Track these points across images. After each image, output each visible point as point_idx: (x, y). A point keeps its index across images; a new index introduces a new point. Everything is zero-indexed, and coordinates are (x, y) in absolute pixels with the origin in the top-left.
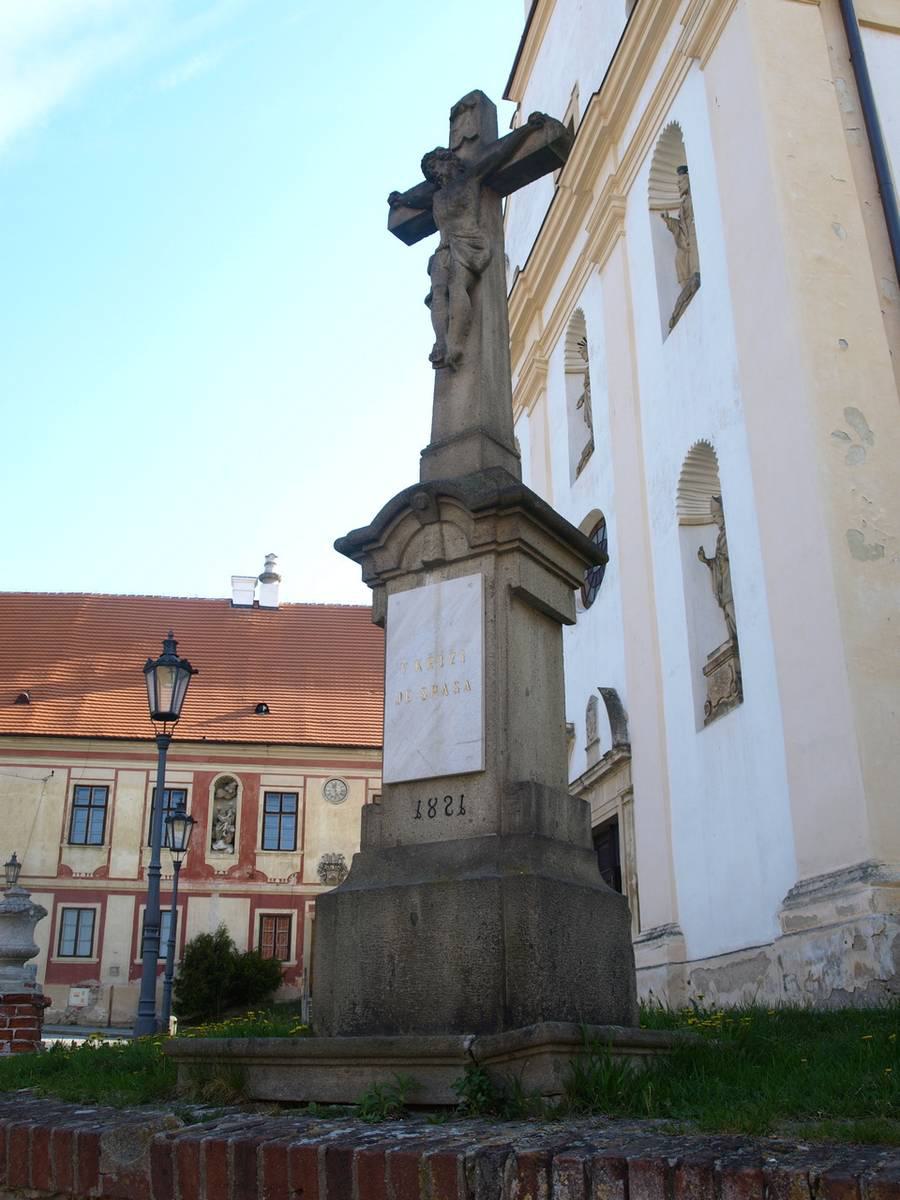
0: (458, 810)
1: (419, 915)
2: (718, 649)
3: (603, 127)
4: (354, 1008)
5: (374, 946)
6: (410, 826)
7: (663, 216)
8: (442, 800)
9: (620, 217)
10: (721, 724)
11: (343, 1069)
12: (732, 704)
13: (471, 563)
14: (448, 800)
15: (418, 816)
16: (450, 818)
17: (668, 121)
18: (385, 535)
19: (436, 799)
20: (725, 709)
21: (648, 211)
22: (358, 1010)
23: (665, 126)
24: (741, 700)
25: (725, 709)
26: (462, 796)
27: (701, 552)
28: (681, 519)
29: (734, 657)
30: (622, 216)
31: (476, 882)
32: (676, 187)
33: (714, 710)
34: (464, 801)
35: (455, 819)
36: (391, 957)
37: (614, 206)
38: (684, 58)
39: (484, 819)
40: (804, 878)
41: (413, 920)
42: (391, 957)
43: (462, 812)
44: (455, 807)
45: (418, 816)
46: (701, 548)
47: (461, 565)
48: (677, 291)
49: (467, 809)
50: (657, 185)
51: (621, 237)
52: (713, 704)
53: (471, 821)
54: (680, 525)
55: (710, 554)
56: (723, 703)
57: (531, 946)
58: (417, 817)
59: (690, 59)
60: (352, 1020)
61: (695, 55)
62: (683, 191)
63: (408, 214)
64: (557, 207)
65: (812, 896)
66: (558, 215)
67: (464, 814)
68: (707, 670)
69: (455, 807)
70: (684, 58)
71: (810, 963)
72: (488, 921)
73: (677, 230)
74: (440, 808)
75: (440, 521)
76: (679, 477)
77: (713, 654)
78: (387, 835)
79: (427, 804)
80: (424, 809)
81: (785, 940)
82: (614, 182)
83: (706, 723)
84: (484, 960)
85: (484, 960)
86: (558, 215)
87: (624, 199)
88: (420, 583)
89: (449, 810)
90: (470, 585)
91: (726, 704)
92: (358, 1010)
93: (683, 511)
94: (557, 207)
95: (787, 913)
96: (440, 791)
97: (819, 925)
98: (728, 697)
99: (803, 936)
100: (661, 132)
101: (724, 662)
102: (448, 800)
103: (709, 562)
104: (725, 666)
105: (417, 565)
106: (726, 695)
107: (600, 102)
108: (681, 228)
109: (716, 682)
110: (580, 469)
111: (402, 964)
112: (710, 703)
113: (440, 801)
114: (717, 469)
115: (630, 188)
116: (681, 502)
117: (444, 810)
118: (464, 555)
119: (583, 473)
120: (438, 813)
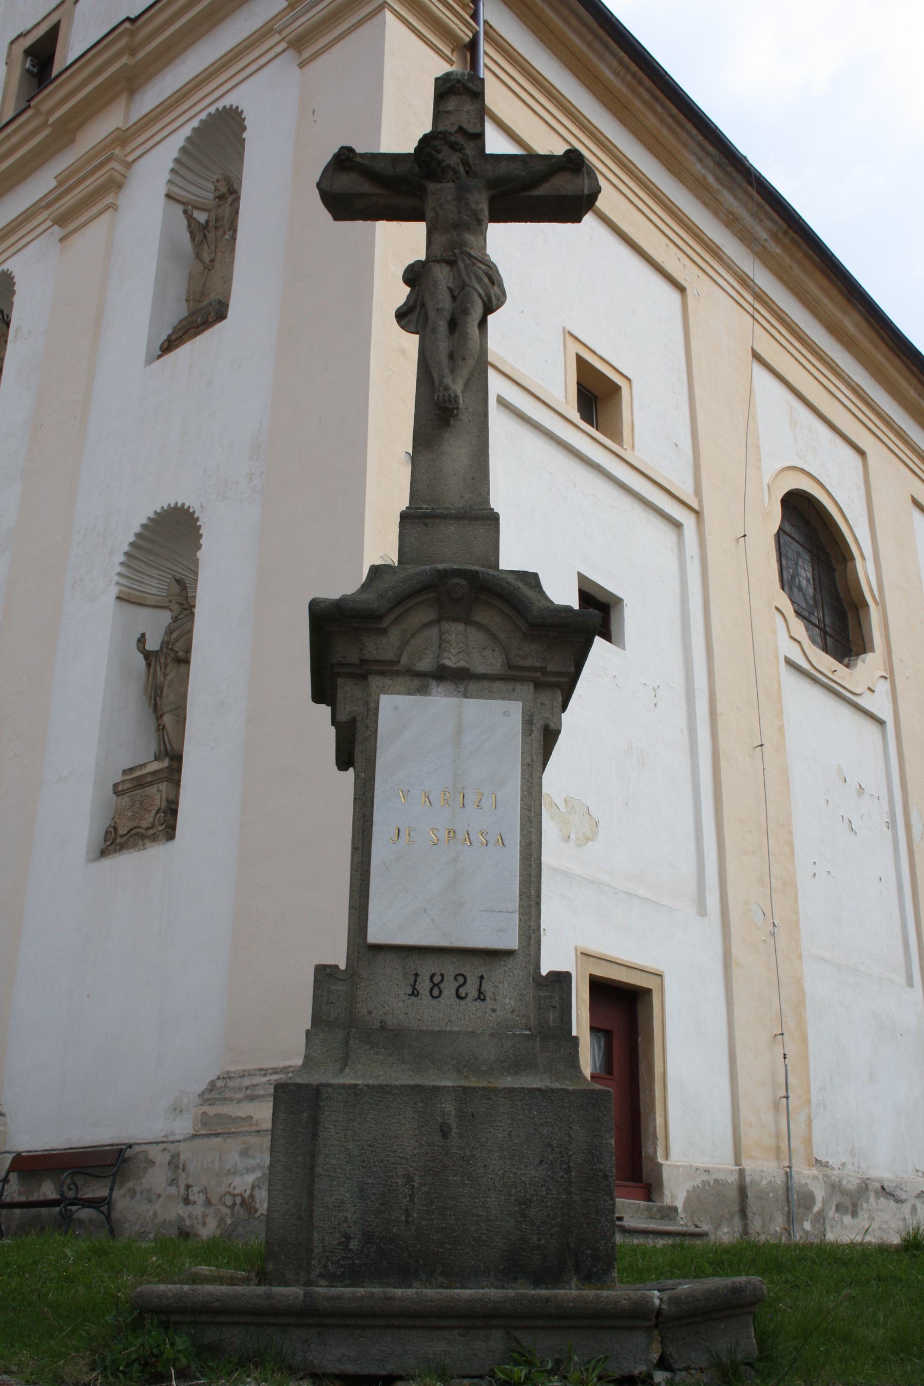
0: (474, 993)
1: (454, 1126)
2: (144, 765)
3: (126, 65)
4: (349, 1243)
5: (382, 1161)
6: (401, 1004)
7: (185, 212)
8: (451, 979)
9: (115, 185)
10: (127, 862)
11: (456, 1332)
12: (154, 838)
13: (498, 685)
14: (461, 980)
15: (415, 993)
16: (462, 1002)
17: (227, 102)
18: (392, 616)
19: (442, 975)
20: (141, 843)
21: (162, 198)
22: (354, 1245)
23: (220, 105)
24: (170, 832)
25: (141, 843)
26: (482, 977)
27: (142, 640)
28: (120, 591)
29: (169, 780)
30: (119, 186)
31: (538, 1093)
32: (213, 187)
33: (119, 840)
34: (484, 985)
35: (471, 1007)
36: (409, 1179)
37: (113, 169)
38: (277, 38)
39: (513, 1011)
40: (232, 1068)
41: (445, 1132)
42: (409, 1179)
43: (481, 996)
44: (471, 989)
45: (415, 993)
46: (143, 635)
47: (486, 684)
48: (177, 311)
49: (489, 994)
50: (183, 171)
51: (111, 210)
52: (121, 832)
53: (494, 1011)
54: (118, 598)
55: (153, 645)
56: (137, 834)
57: (606, 1177)
58: (413, 994)
59: (283, 45)
60: (343, 1258)
61: (298, 43)
62: (217, 193)
63: (347, 182)
64: (15, 132)
65: (249, 1092)
66: (14, 140)
67: (417, 996)
68: (120, 788)
69: (471, 989)
70: (277, 38)
71: (234, 1172)
72: (554, 1143)
73: (199, 237)
74: (449, 988)
75: (468, 622)
76: (132, 539)
77: (132, 770)
78: (364, 1011)
79: (427, 981)
80: (424, 986)
81: (198, 1142)
82: (122, 138)
83: (103, 853)
84: (548, 1189)
85: (548, 1189)
86: (14, 140)
87: (129, 165)
88: (423, 690)
89: (462, 992)
90: (506, 713)
91: (143, 837)
92: (354, 1245)
93: (124, 581)
94: (15, 132)
95: (205, 1108)
96: (449, 968)
97: (255, 1128)
98: (147, 829)
99: (229, 1140)
100: (212, 110)
101: (150, 784)
102: (461, 980)
103: (147, 655)
104: (153, 790)
105: (425, 664)
106: (144, 824)
107: (132, 34)
108: (205, 235)
109: (132, 806)
110: (169, 346)
111: (425, 1189)
112: (115, 829)
113: (449, 978)
114: (199, 547)
115: (140, 157)
116: (125, 571)
117: (454, 992)
118: (495, 672)
119: (185, 350)
120: (446, 993)
